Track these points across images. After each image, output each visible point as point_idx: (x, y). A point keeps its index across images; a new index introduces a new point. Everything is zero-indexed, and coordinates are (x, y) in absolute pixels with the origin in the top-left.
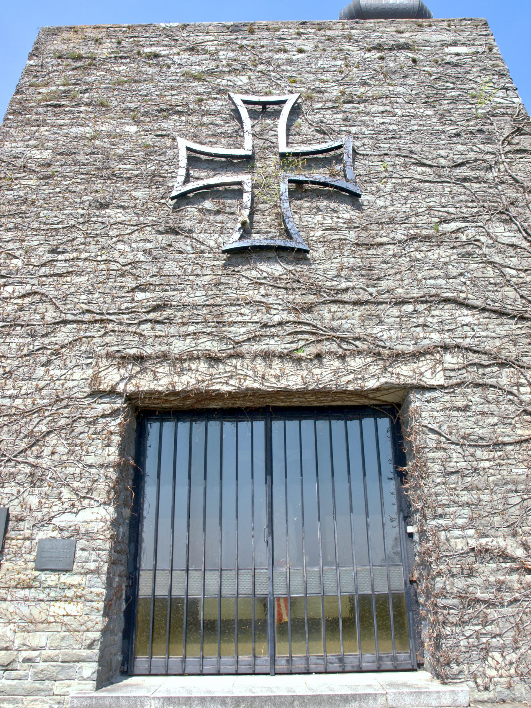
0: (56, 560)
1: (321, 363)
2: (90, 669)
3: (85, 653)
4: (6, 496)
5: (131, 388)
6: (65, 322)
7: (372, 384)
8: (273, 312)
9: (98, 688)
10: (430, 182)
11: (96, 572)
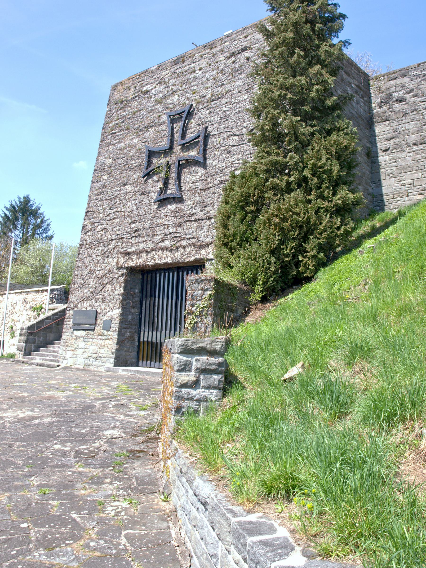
0: (107, 327)
1: (178, 250)
2: (112, 360)
3: (112, 356)
4: (424, 297)
5: (126, 266)
6: (112, 240)
7: (192, 259)
8: (169, 228)
9: (114, 366)
10: (236, 146)
11: (115, 331)
